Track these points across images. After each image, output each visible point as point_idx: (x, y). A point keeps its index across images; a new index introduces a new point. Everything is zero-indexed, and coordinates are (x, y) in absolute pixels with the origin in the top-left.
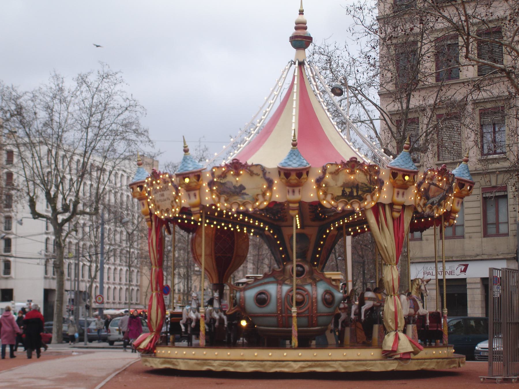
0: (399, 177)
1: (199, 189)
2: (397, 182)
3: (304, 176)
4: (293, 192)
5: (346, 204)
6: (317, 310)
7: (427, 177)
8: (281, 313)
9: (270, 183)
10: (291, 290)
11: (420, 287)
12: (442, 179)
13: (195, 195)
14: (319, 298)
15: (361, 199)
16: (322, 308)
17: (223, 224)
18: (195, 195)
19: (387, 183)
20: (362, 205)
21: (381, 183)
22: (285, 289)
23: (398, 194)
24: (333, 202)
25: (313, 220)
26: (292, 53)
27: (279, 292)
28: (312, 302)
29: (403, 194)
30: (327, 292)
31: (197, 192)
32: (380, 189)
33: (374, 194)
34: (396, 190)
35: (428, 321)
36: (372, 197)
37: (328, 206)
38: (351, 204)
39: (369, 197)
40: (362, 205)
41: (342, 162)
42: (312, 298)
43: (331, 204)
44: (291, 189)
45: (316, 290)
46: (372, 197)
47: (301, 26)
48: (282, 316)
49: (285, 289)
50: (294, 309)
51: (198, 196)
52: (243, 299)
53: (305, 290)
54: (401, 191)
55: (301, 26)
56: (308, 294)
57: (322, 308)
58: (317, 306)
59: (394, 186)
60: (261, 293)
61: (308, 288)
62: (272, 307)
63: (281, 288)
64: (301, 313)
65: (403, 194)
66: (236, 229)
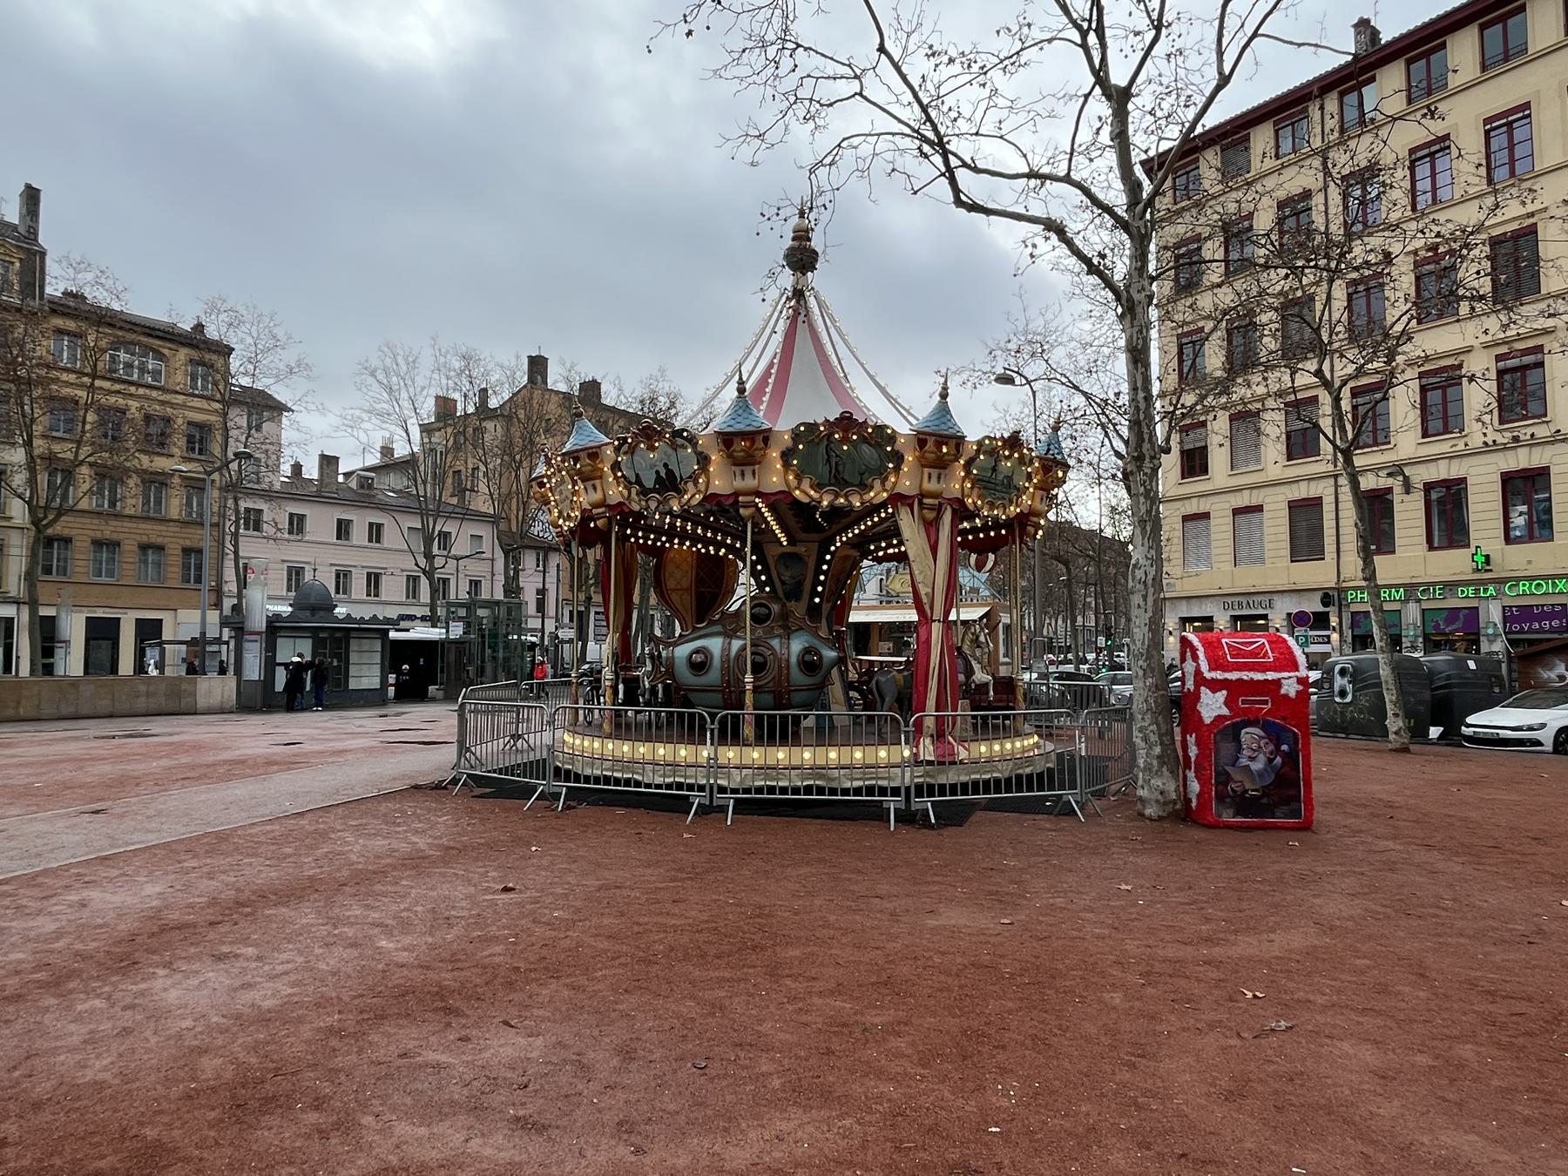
0: (930, 445)
1: (601, 477)
2: (927, 455)
3: (759, 443)
4: (743, 474)
5: (837, 496)
6: (788, 681)
7: (983, 449)
8: (729, 686)
9: (703, 460)
10: (743, 648)
11: (978, 637)
12: (1010, 456)
13: (595, 488)
14: (794, 660)
15: (864, 487)
16: (797, 676)
17: (664, 539)
18: (595, 488)
19: (909, 458)
20: (866, 497)
21: (898, 458)
22: (736, 644)
23: (930, 478)
24: (812, 493)
25: (806, 530)
26: (787, 279)
27: (726, 650)
28: (780, 666)
29: (939, 478)
30: (807, 651)
31: (597, 482)
32: (897, 469)
33: (886, 478)
34: (926, 470)
35: (992, 693)
36: (883, 484)
37: (806, 500)
38: (846, 497)
39: (877, 484)
40: (866, 497)
41: (827, 421)
42: (780, 660)
43: (810, 496)
44: (738, 469)
45: (788, 648)
46: (883, 484)
47: (802, 235)
48: (731, 692)
49: (736, 644)
50: (749, 678)
51: (599, 488)
52: (671, 659)
53: (771, 648)
54: (935, 472)
55: (802, 235)
56: (774, 653)
57: (797, 676)
58: (788, 674)
59: (923, 463)
60: (697, 651)
61: (775, 643)
62: (713, 676)
63: (730, 643)
64: (760, 687)
65: (939, 478)
66: (708, 551)
